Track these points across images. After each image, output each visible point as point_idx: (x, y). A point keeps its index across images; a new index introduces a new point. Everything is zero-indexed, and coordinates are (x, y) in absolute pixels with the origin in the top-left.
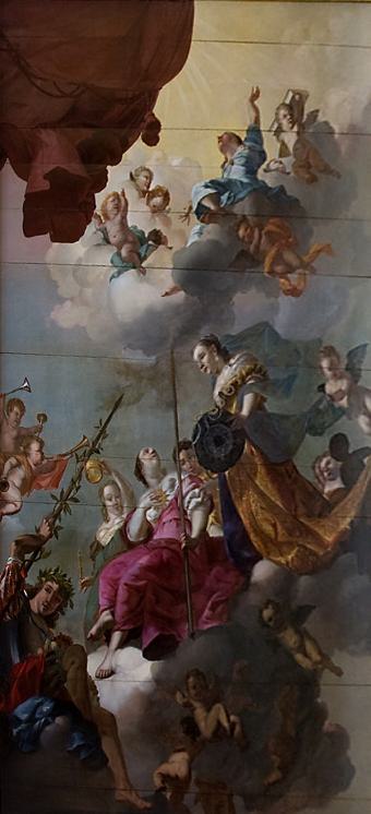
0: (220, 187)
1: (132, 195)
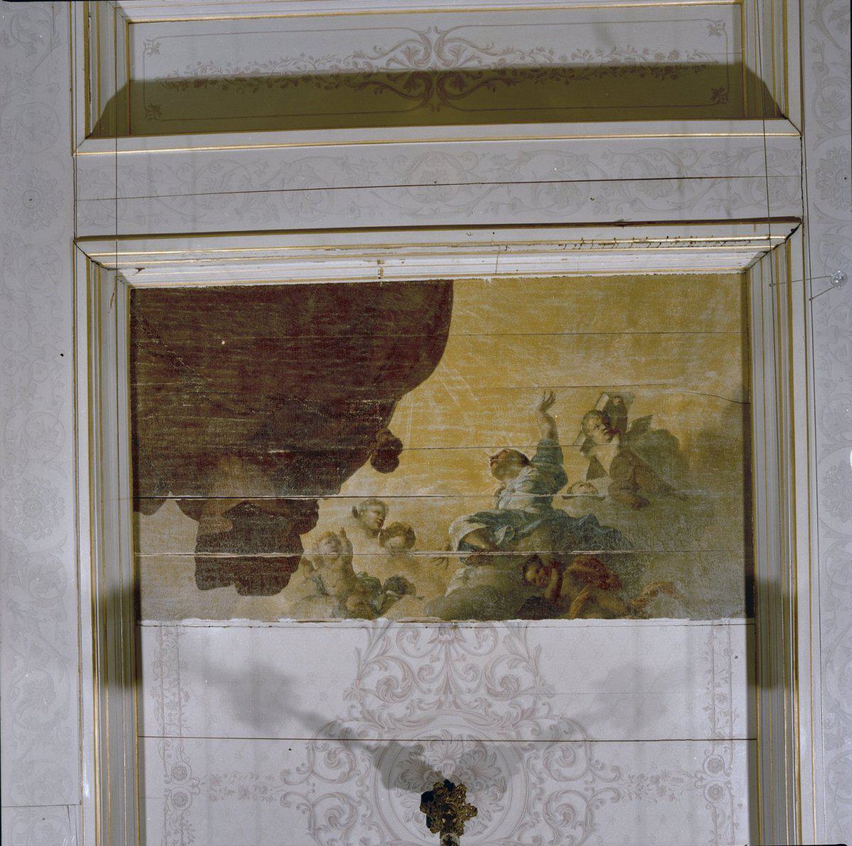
0: (489, 521)
1: (356, 537)
